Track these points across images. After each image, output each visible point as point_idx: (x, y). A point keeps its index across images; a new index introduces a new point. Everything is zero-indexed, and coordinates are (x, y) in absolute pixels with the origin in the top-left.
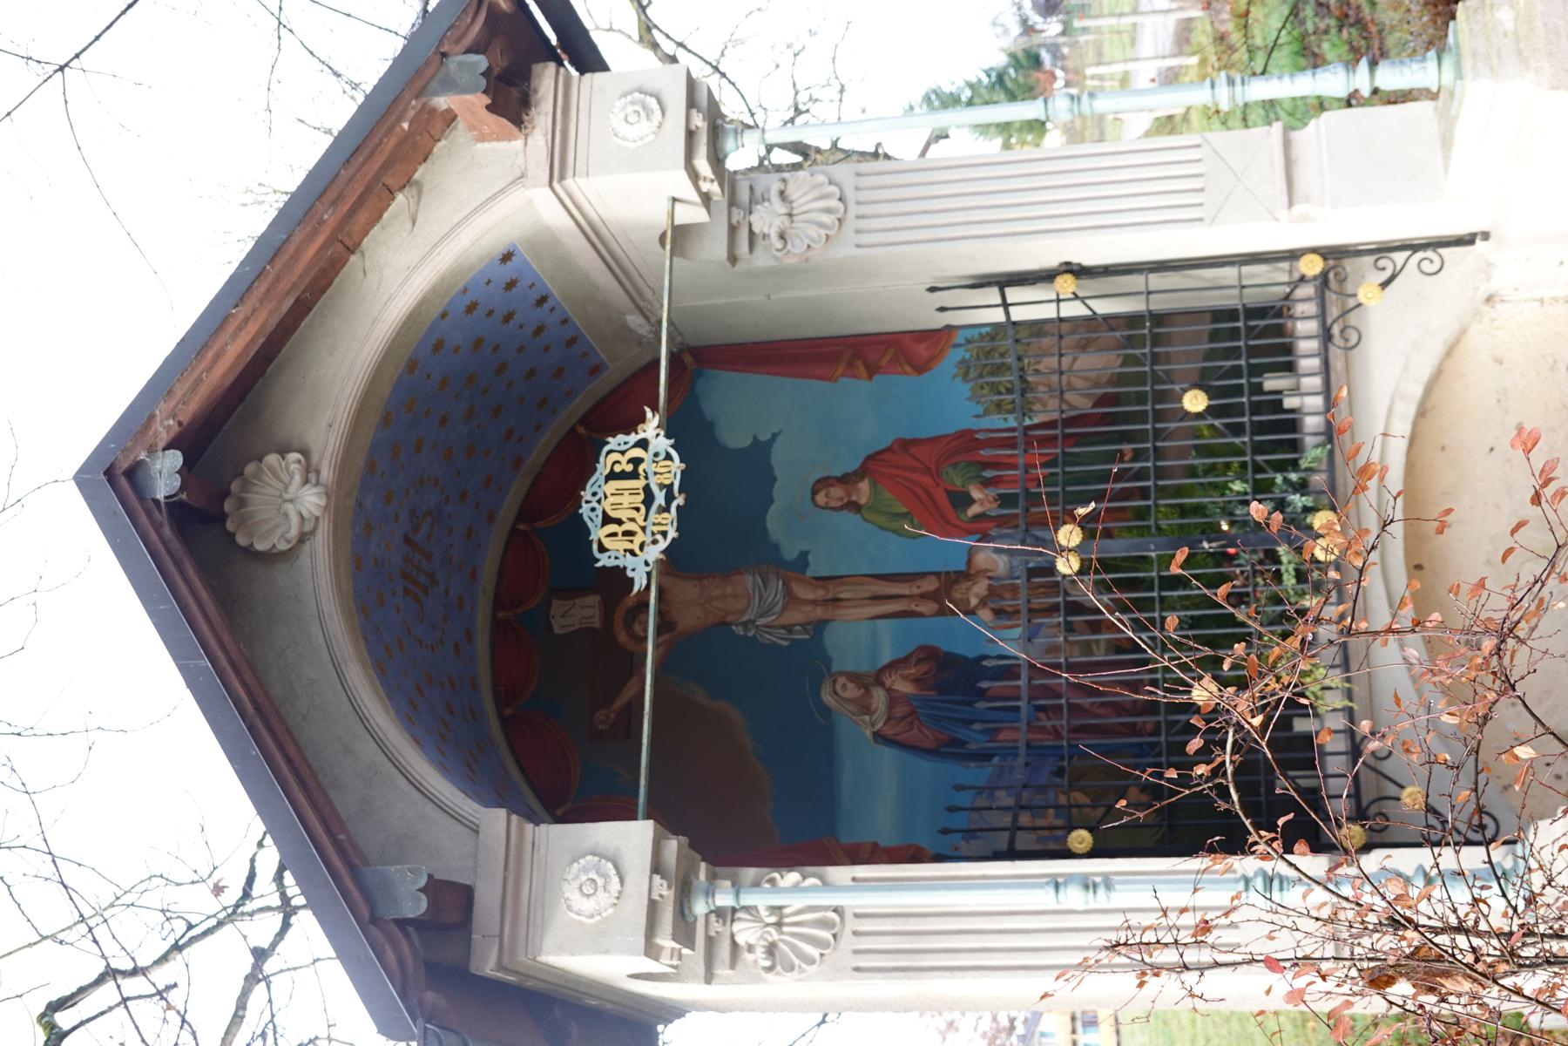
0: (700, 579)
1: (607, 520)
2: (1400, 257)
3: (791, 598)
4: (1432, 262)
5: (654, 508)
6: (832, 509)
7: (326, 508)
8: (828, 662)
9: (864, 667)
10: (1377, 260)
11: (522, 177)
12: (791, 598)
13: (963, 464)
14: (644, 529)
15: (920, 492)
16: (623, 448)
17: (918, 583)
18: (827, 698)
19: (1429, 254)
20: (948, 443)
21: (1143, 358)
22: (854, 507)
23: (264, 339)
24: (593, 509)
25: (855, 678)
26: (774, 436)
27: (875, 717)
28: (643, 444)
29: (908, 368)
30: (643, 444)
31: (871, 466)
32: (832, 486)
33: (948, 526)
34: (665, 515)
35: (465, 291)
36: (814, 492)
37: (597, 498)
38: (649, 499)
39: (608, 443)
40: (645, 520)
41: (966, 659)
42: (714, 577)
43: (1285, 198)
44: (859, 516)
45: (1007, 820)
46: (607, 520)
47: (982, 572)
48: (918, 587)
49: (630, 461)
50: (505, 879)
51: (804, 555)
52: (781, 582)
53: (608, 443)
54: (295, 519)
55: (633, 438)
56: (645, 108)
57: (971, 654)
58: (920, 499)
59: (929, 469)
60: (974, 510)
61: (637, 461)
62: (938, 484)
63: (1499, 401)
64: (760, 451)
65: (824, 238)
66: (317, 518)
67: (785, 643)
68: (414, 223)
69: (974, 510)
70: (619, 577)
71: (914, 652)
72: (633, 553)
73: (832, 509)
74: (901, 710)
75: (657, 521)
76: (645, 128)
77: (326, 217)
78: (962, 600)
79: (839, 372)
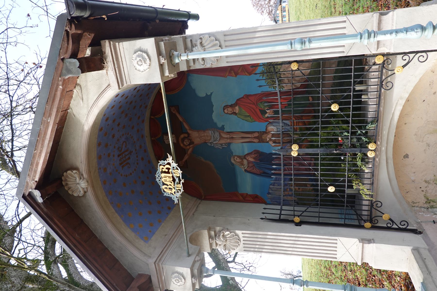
0: (198, 131)
1: (164, 184)
2: (411, 56)
3: (221, 137)
4: (423, 57)
5: (176, 183)
6: (229, 114)
7: (88, 185)
8: (232, 153)
9: (241, 155)
10: (403, 57)
11: (109, 85)
12: (221, 137)
13: (263, 102)
14: (174, 188)
15: (252, 110)
16: (164, 164)
17: (253, 134)
18: (233, 161)
19: (424, 54)
20: (259, 96)
21: (319, 91)
22: (235, 113)
23: (49, 154)
24: (159, 180)
25: (239, 157)
26: (211, 93)
27: (244, 166)
28: (169, 164)
29: (246, 73)
31: (238, 102)
32: (228, 108)
33: (261, 120)
34: (179, 185)
35: (104, 115)
36: (224, 109)
37: (160, 177)
38: (174, 180)
39: (159, 162)
40: (174, 186)
41: (266, 153)
42: (201, 131)
43: (376, 46)
44: (236, 116)
45: (278, 212)
46: (164, 184)
47: (269, 132)
48: (253, 135)
49: (166, 168)
50: (158, 276)
51: (223, 126)
52: (218, 133)
53: (159, 162)
54: (81, 190)
55: (166, 162)
56: (143, 58)
57: (268, 152)
58: (252, 112)
59: (254, 104)
61: (168, 169)
62: (257, 108)
63: (430, 84)
64: (208, 97)
65: (216, 60)
66: (87, 188)
67: (221, 148)
68: (83, 99)
70: (169, 199)
71: (253, 151)
72: (172, 194)
73: (229, 114)
74: (251, 165)
75: (177, 186)
76: (145, 66)
77: (49, 121)
78: (265, 139)
79: (227, 74)
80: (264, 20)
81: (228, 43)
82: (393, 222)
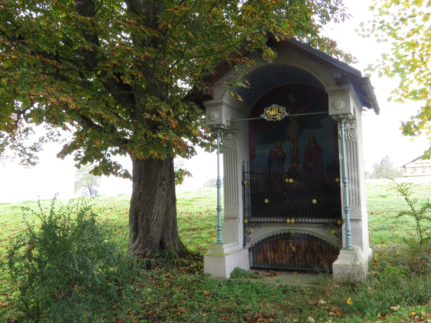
18: (278, 142)
30: (284, 113)
55: (285, 111)
60: (309, 164)
69: (309, 164)
80: (5, 217)
81: (348, 144)
82: (249, 234)
